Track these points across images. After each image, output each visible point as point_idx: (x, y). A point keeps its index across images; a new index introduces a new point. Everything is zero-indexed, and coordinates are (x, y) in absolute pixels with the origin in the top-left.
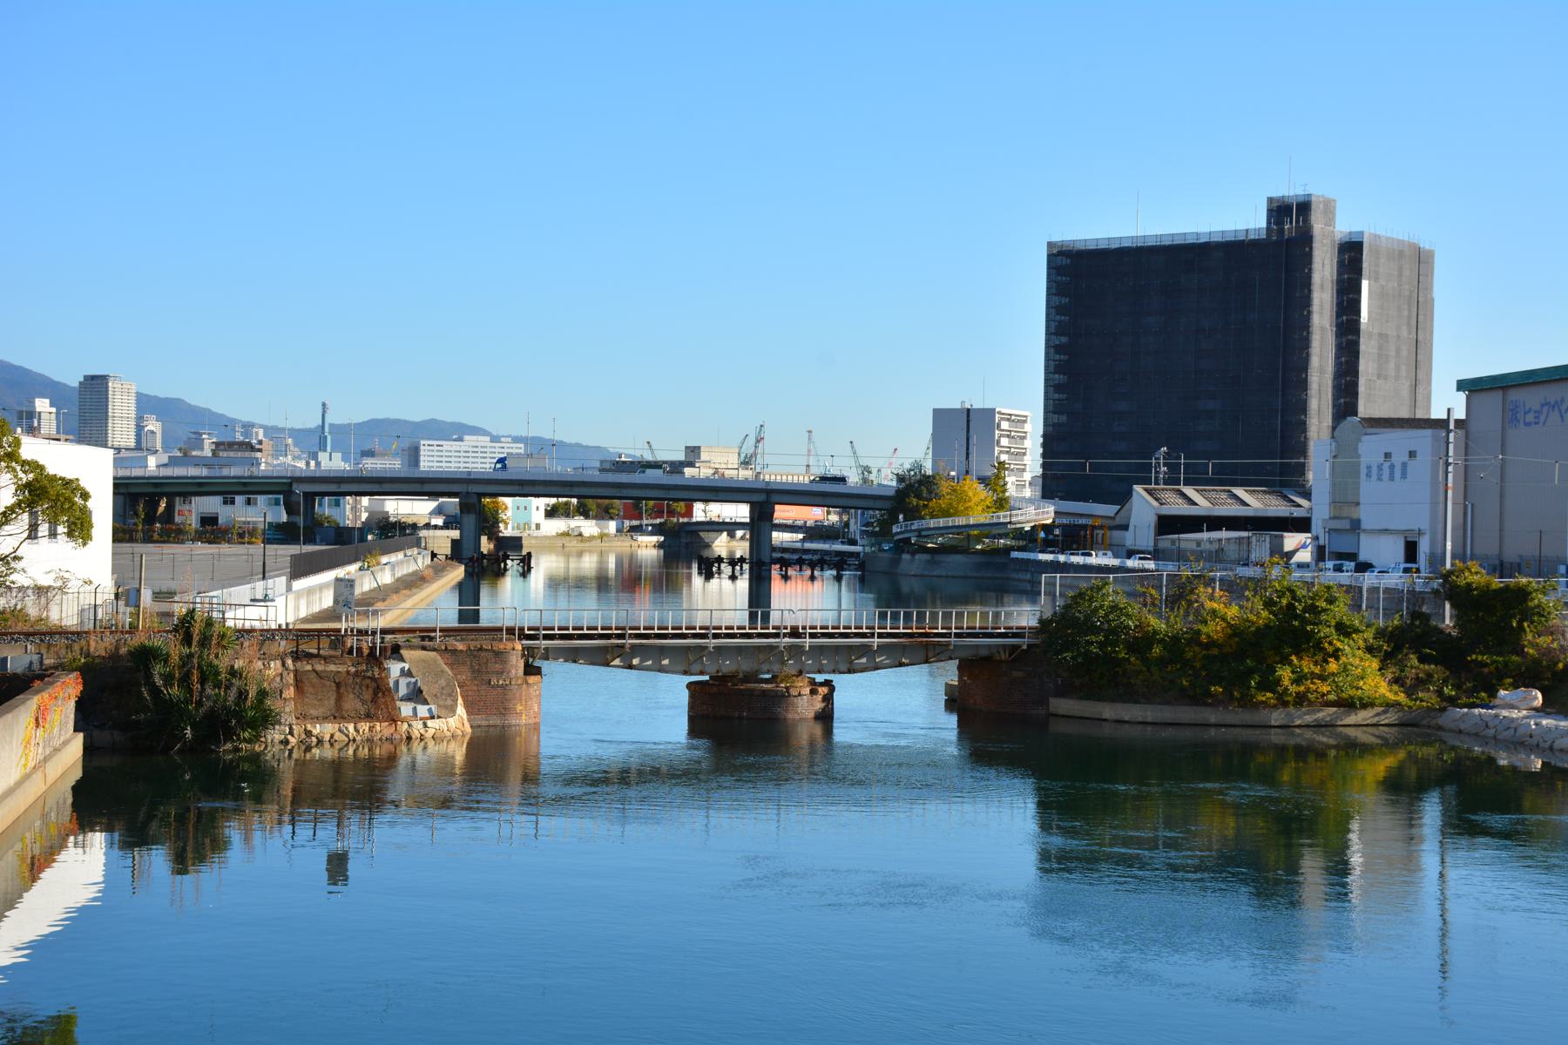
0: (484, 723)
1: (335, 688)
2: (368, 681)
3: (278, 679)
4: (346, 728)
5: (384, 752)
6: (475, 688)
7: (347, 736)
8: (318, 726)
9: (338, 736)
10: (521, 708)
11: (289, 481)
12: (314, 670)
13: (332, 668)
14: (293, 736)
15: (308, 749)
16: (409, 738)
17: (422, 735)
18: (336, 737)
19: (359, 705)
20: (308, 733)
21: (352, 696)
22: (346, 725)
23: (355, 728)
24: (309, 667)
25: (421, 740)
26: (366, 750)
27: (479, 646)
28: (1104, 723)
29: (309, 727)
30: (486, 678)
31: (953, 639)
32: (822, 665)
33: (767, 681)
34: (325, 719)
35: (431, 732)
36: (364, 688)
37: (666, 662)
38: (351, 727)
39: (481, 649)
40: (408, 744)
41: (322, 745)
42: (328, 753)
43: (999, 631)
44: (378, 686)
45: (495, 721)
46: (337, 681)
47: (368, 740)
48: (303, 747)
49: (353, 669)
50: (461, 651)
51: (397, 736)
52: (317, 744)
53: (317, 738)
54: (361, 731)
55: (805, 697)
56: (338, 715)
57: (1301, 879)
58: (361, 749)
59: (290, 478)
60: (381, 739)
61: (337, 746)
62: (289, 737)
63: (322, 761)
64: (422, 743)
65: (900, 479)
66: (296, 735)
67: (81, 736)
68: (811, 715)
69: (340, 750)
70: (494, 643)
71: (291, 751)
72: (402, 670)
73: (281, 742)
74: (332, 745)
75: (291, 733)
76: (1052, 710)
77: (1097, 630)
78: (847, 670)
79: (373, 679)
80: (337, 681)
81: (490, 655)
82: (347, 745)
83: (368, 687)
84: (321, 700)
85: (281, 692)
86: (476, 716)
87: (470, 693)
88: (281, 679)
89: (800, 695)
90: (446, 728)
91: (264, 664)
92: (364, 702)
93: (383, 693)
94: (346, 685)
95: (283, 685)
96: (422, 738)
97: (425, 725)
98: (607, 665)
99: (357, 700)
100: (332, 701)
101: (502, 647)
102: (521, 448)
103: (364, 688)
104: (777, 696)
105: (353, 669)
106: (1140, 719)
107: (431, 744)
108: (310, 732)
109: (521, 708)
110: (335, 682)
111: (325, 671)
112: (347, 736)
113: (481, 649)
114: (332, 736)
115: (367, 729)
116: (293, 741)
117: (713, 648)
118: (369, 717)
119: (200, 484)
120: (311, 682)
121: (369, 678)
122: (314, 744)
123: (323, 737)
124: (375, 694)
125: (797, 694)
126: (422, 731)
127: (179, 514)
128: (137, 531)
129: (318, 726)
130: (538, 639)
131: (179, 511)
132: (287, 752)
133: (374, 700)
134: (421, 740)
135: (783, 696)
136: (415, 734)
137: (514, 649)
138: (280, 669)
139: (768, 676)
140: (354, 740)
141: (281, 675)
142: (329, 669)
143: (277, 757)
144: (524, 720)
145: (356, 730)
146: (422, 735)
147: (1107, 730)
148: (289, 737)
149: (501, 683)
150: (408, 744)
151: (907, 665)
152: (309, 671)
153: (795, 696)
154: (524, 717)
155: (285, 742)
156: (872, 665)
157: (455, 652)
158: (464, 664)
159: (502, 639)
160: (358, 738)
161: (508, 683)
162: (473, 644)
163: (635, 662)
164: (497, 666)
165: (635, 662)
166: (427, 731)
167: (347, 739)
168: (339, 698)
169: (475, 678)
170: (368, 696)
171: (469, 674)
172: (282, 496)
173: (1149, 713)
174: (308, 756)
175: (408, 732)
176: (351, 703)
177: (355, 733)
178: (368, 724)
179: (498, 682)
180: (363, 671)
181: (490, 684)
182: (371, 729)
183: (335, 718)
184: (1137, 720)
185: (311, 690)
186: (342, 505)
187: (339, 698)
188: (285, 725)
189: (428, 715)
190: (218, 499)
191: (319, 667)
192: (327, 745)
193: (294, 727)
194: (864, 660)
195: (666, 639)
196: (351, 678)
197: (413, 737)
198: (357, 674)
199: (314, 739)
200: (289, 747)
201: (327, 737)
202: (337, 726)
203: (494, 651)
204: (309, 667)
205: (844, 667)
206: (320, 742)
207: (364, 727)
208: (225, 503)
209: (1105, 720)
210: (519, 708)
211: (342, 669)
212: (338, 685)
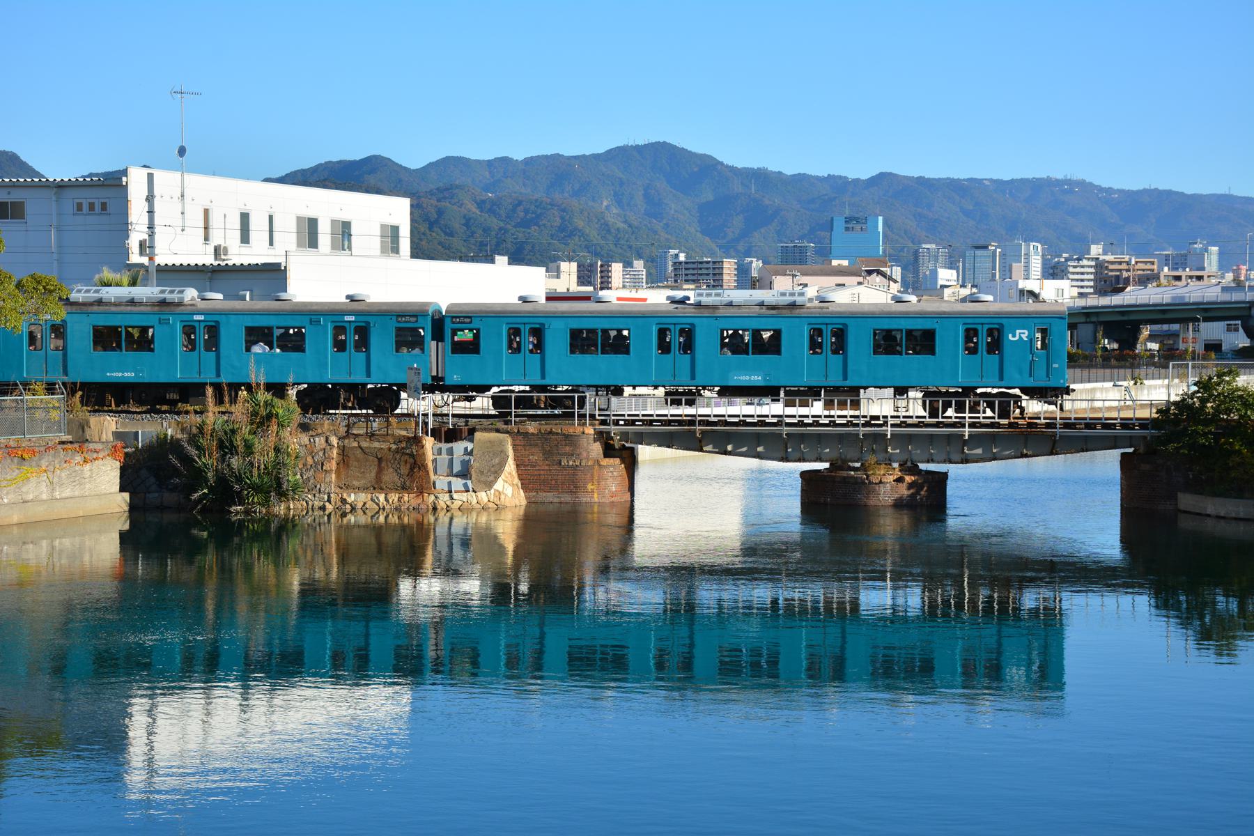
0: (556, 500)
1: (376, 463)
2: (406, 457)
3: (321, 453)
6: (547, 468)
7: (378, 505)
8: (353, 495)
9: (370, 504)
10: (592, 487)
11: (1248, 305)
12: (360, 447)
13: (376, 445)
15: (344, 515)
16: (435, 509)
17: (448, 506)
18: (367, 506)
19: (396, 478)
20: (344, 501)
21: (391, 470)
23: (386, 498)
24: (355, 444)
25: (448, 511)
26: (396, 518)
27: (549, 430)
28: (1208, 518)
29: (345, 496)
30: (556, 458)
34: (365, 489)
35: (457, 504)
36: (402, 463)
37: (760, 449)
38: (382, 497)
39: (551, 432)
40: (434, 514)
41: (356, 512)
42: (363, 519)
45: (567, 498)
46: (379, 457)
47: (396, 509)
48: (339, 513)
49: (394, 447)
50: (533, 434)
51: (424, 507)
52: (351, 511)
53: (351, 505)
54: (390, 501)
58: (390, 516)
59: (1249, 302)
60: (408, 509)
61: (370, 514)
62: (327, 504)
64: (449, 514)
66: (333, 504)
67: (126, 495)
68: (890, 501)
70: (564, 427)
71: (329, 516)
72: (466, 449)
73: (320, 508)
74: (364, 513)
75: (329, 501)
76: (1182, 506)
77: (1207, 422)
78: (960, 461)
79: (411, 455)
80: (379, 457)
82: (378, 512)
83: (406, 462)
85: (323, 464)
88: (324, 453)
89: (881, 482)
90: (475, 501)
91: (310, 440)
92: (400, 475)
93: (419, 468)
95: (326, 458)
96: (448, 509)
97: (452, 498)
98: (701, 450)
100: (373, 474)
101: (571, 431)
102: (1153, 263)
103: (402, 463)
104: (856, 483)
105: (394, 447)
106: (1234, 515)
108: (345, 500)
109: (592, 487)
110: (377, 457)
112: (378, 505)
113: (551, 432)
115: (396, 499)
116: (329, 507)
117: (863, 435)
118: (404, 488)
119: (1164, 311)
121: (408, 454)
123: (356, 505)
124: (412, 469)
125: (877, 482)
126: (448, 503)
127: (1183, 342)
128: (1096, 357)
129: (353, 495)
131: (1183, 339)
132: (326, 518)
134: (448, 511)
135: (863, 483)
137: (583, 433)
139: (858, 465)
140: (384, 509)
141: (324, 449)
145: (387, 500)
146: (448, 506)
148: (327, 504)
149: (571, 463)
150: (434, 514)
153: (876, 484)
154: (596, 495)
155: (323, 508)
156: (990, 456)
158: (536, 445)
159: (586, 423)
160: (388, 507)
162: (548, 428)
163: (730, 448)
164: (567, 448)
165: (730, 448)
169: (546, 459)
170: (405, 470)
172: (1239, 322)
173: (1241, 509)
174: (345, 520)
175: (434, 503)
176: (390, 476)
177: (385, 503)
178: (397, 495)
180: (403, 448)
181: (560, 464)
182: (400, 499)
183: (374, 489)
184: (1231, 516)
185: (355, 463)
186: (928, 325)
188: (325, 493)
190: (1222, 325)
191: (364, 444)
192: (360, 512)
193: (332, 495)
194: (979, 451)
195: (716, 426)
196: (391, 454)
197: (439, 507)
198: (397, 451)
199: (348, 506)
200: (327, 512)
201: (360, 505)
202: (369, 496)
203: (564, 435)
204: (355, 444)
205: (955, 457)
206: (353, 509)
207: (394, 497)
208: (1229, 330)
209: (1209, 516)
210: (590, 487)
211: (384, 446)
212: (380, 460)
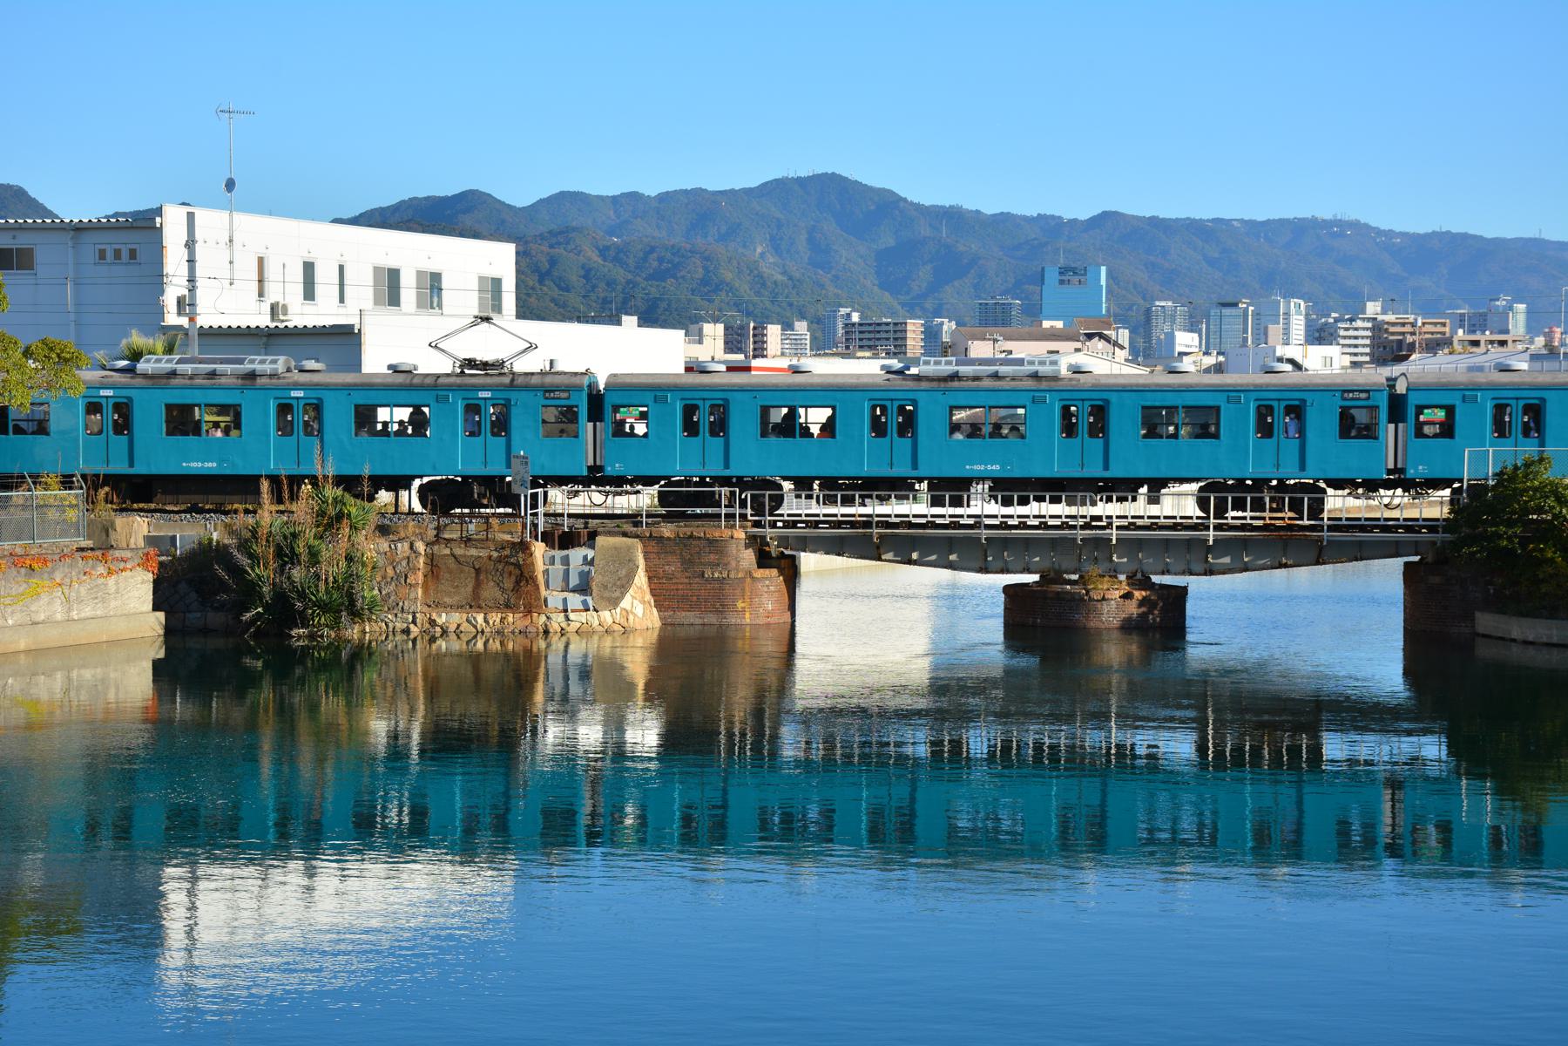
1: (474, 575)
2: (511, 568)
3: (404, 563)
4: (475, 618)
5: (519, 649)
6: (687, 581)
7: (475, 627)
8: (444, 615)
9: (465, 626)
10: (743, 605)
13: (473, 552)
14: (416, 625)
15: (433, 640)
16: (546, 632)
17: (562, 629)
18: (462, 628)
19: (498, 594)
20: (432, 623)
21: (492, 584)
22: (474, 615)
24: (447, 551)
26: (498, 643)
27: (689, 533)
29: (434, 616)
30: (698, 569)
31: (1325, 534)
32: (1167, 563)
33: (1071, 582)
34: (460, 607)
35: (574, 626)
37: (953, 557)
38: (480, 618)
39: (691, 537)
41: (447, 636)
42: (456, 646)
43: (895, 508)
44: (522, 573)
45: (712, 619)
46: (477, 567)
47: (498, 632)
48: (427, 638)
49: (495, 554)
50: (669, 538)
51: (532, 629)
52: (442, 636)
53: (442, 628)
54: (491, 622)
55: (1113, 602)
56: (475, 603)
57: (1337, 827)
58: (491, 641)
60: (513, 632)
61: (465, 638)
62: (412, 626)
63: (448, 654)
64: (564, 639)
65: (619, 323)
67: (161, 615)
68: (1116, 623)
69: (468, 643)
70: (707, 530)
71: (414, 641)
72: (585, 557)
75: (414, 622)
76: (1480, 630)
79: (517, 565)
80: (477, 567)
81: (704, 542)
82: (475, 637)
83: (510, 574)
84: (457, 586)
86: (688, 613)
87: (681, 587)
88: (408, 563)
89: (1104, 599)
90: (597, 622)
92: (503, 590)
93: (527, 581)
94: (487, 571)
96: (563, 632)
97: (568, 619)
98: (879, 559)
99: (497, 589)
100: (470, 589)
101: (717, 534)
102: (1444, 325)
105: (495, 554)
106: (1545, 640)
107: (574, 639)
108: (435, 621)
109: (743, 605)
111: (465, 556)
112: (475, 627)
113: (691, 537)
114: (459, 626)
115: (498, 620)
116: (415, 630)
118: (508, 606)
120: (448, 568)
121: (512, 564)
122: (437, 635)
124: (517, 583)
125: (1099, 598)
126: (564, 625)
129: (444, 615)
130: (764, 527)
133: (517, 587)
135: (1082, 600)
136: (554, 626)
137: (732, 537)
138: (408, 552)
139: (1075, 577)
140: (483, 632)
141: (408, 558)
142: (468, 554)
143: (399, 648)
144: (748, 619)
145: (486, 621)
146: (562, 629)
147: (1516, 654)
148: (412, 626)
149: (716, 575)
151: (1291, 566)
152: (448, 555)
153: (1098, 601)
154: (747, 615)
155: (407, 631)
157: (660, 539)
159: (735, 525)
160: (487, 630)
161: (725, 575)
162: (688, 531)
163: (915, 556)
165: (915, 556)
166: (569, 625)
167: (474, 630)
168: (478, 585)
170: (508, 584)
171: (679, 565)
173: (1555, 632)
175: (546, 625)
176: (490, 592)
179: (713, 574)
180: (507, 556)
181: (703, 576)
183: (471, 607)
184: (1542, 640)
185: (447, 576)
187: (478, 585)
189: (582, 608)
192: (452, 636)
193: (418, 615)
195: (898, 528)
197: (551, 630)
198: (499, 560)
200: (412, 636)
201: (452, 628)
202: (465, 616)
203: (708, 539)
204: (447, 551)
206: (444, 632)
207: (495, 618)
209: (1514, 640)
210: (740, 605)
211: (484, 553)
212: (478, 571)
